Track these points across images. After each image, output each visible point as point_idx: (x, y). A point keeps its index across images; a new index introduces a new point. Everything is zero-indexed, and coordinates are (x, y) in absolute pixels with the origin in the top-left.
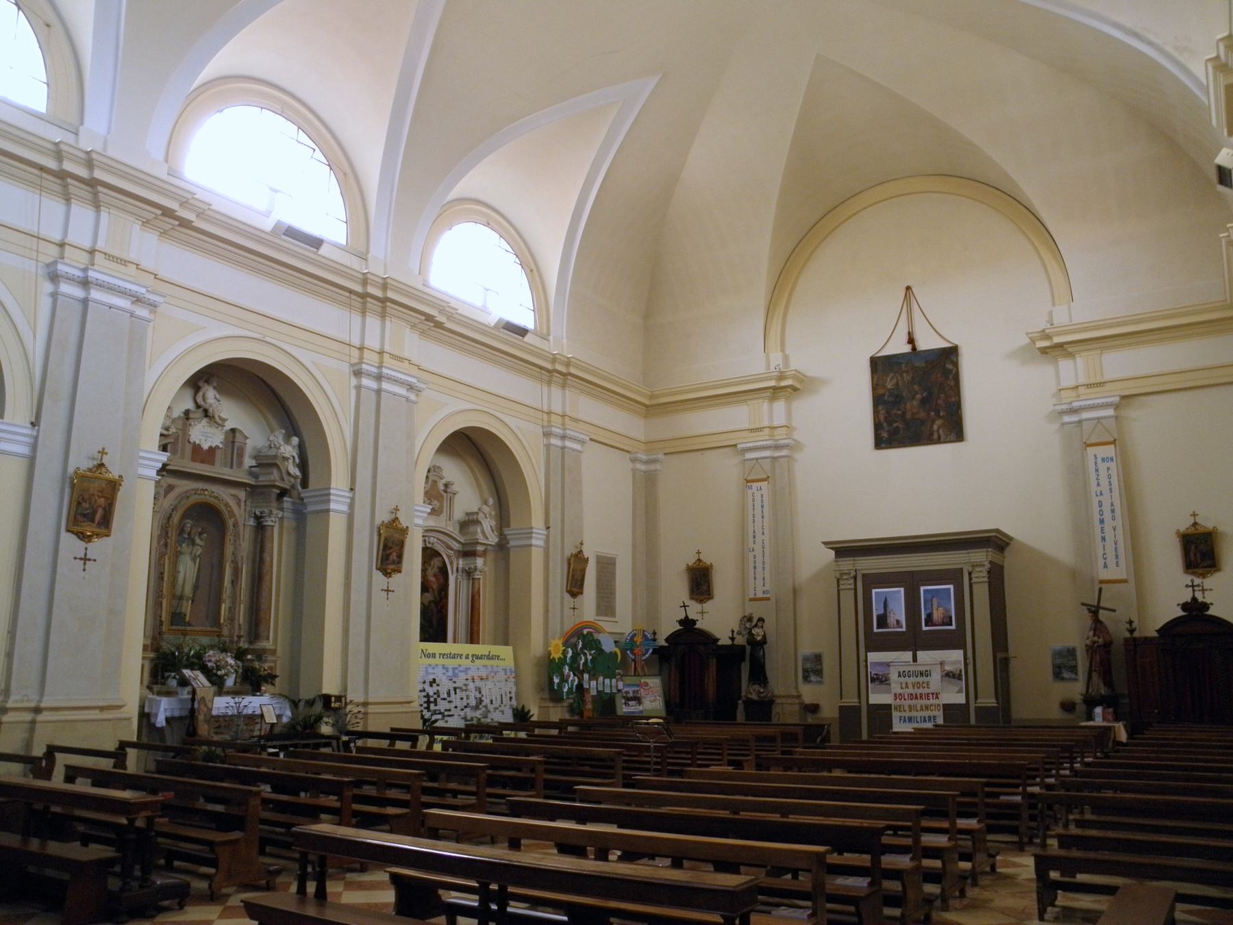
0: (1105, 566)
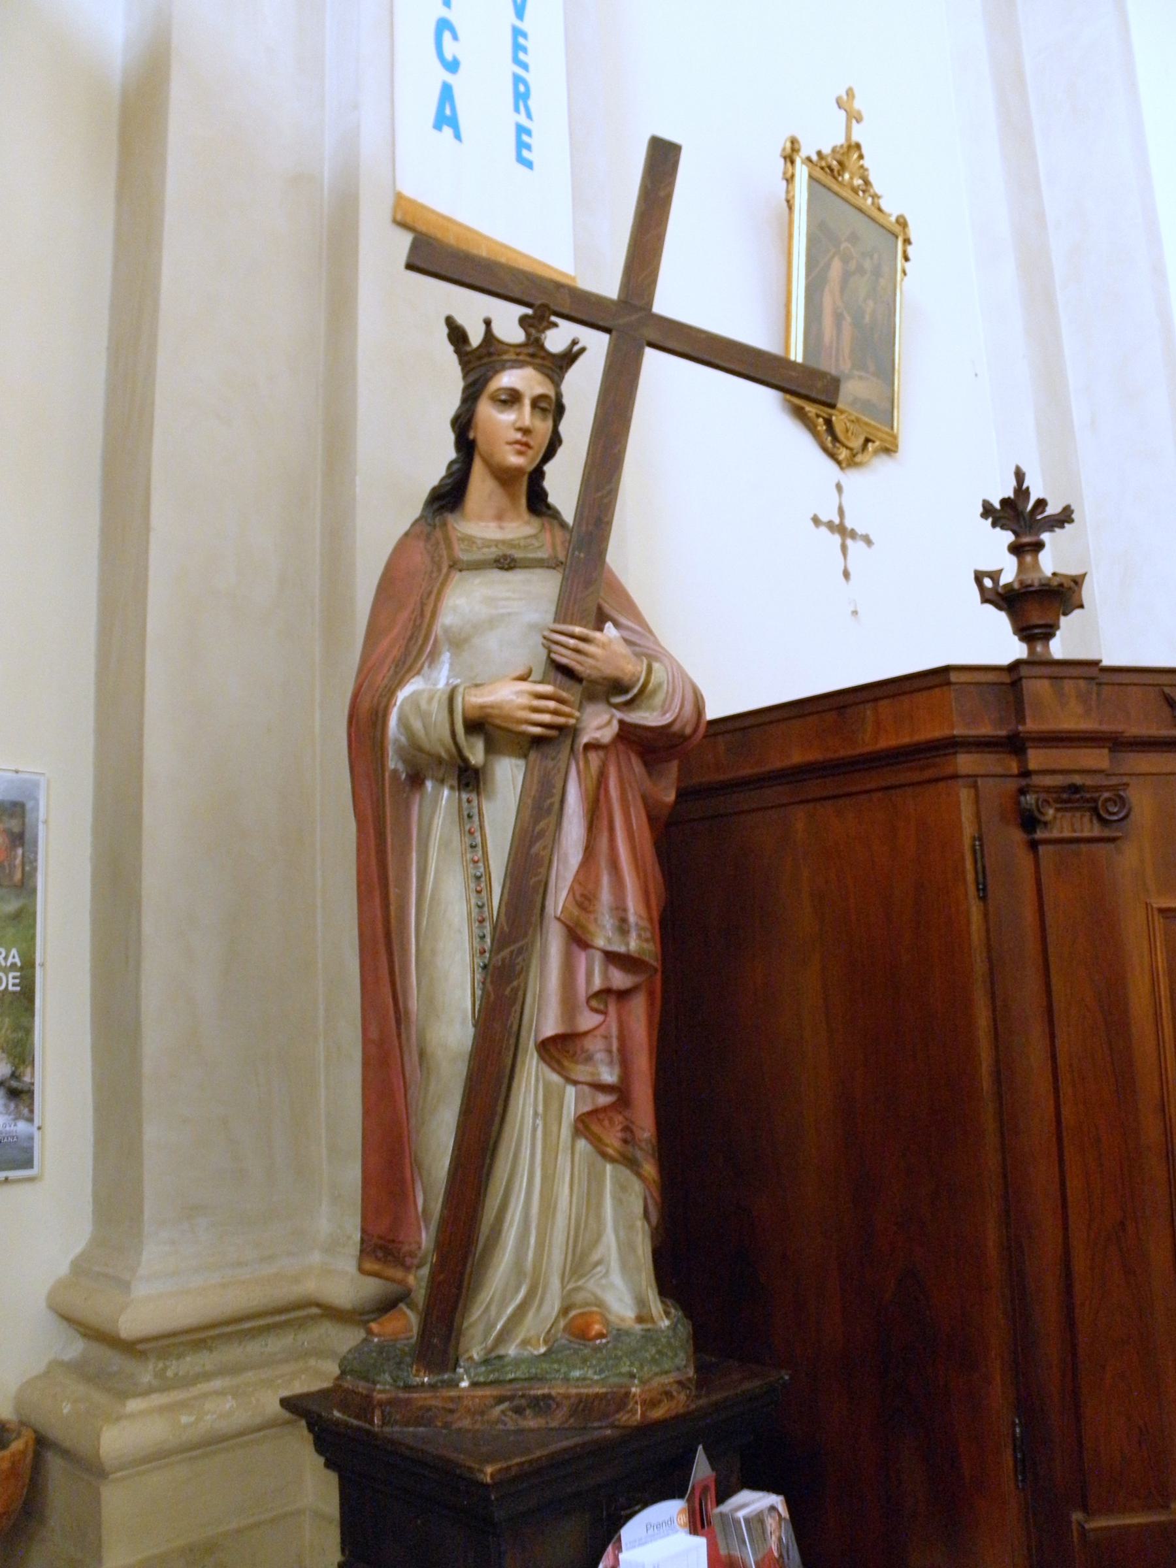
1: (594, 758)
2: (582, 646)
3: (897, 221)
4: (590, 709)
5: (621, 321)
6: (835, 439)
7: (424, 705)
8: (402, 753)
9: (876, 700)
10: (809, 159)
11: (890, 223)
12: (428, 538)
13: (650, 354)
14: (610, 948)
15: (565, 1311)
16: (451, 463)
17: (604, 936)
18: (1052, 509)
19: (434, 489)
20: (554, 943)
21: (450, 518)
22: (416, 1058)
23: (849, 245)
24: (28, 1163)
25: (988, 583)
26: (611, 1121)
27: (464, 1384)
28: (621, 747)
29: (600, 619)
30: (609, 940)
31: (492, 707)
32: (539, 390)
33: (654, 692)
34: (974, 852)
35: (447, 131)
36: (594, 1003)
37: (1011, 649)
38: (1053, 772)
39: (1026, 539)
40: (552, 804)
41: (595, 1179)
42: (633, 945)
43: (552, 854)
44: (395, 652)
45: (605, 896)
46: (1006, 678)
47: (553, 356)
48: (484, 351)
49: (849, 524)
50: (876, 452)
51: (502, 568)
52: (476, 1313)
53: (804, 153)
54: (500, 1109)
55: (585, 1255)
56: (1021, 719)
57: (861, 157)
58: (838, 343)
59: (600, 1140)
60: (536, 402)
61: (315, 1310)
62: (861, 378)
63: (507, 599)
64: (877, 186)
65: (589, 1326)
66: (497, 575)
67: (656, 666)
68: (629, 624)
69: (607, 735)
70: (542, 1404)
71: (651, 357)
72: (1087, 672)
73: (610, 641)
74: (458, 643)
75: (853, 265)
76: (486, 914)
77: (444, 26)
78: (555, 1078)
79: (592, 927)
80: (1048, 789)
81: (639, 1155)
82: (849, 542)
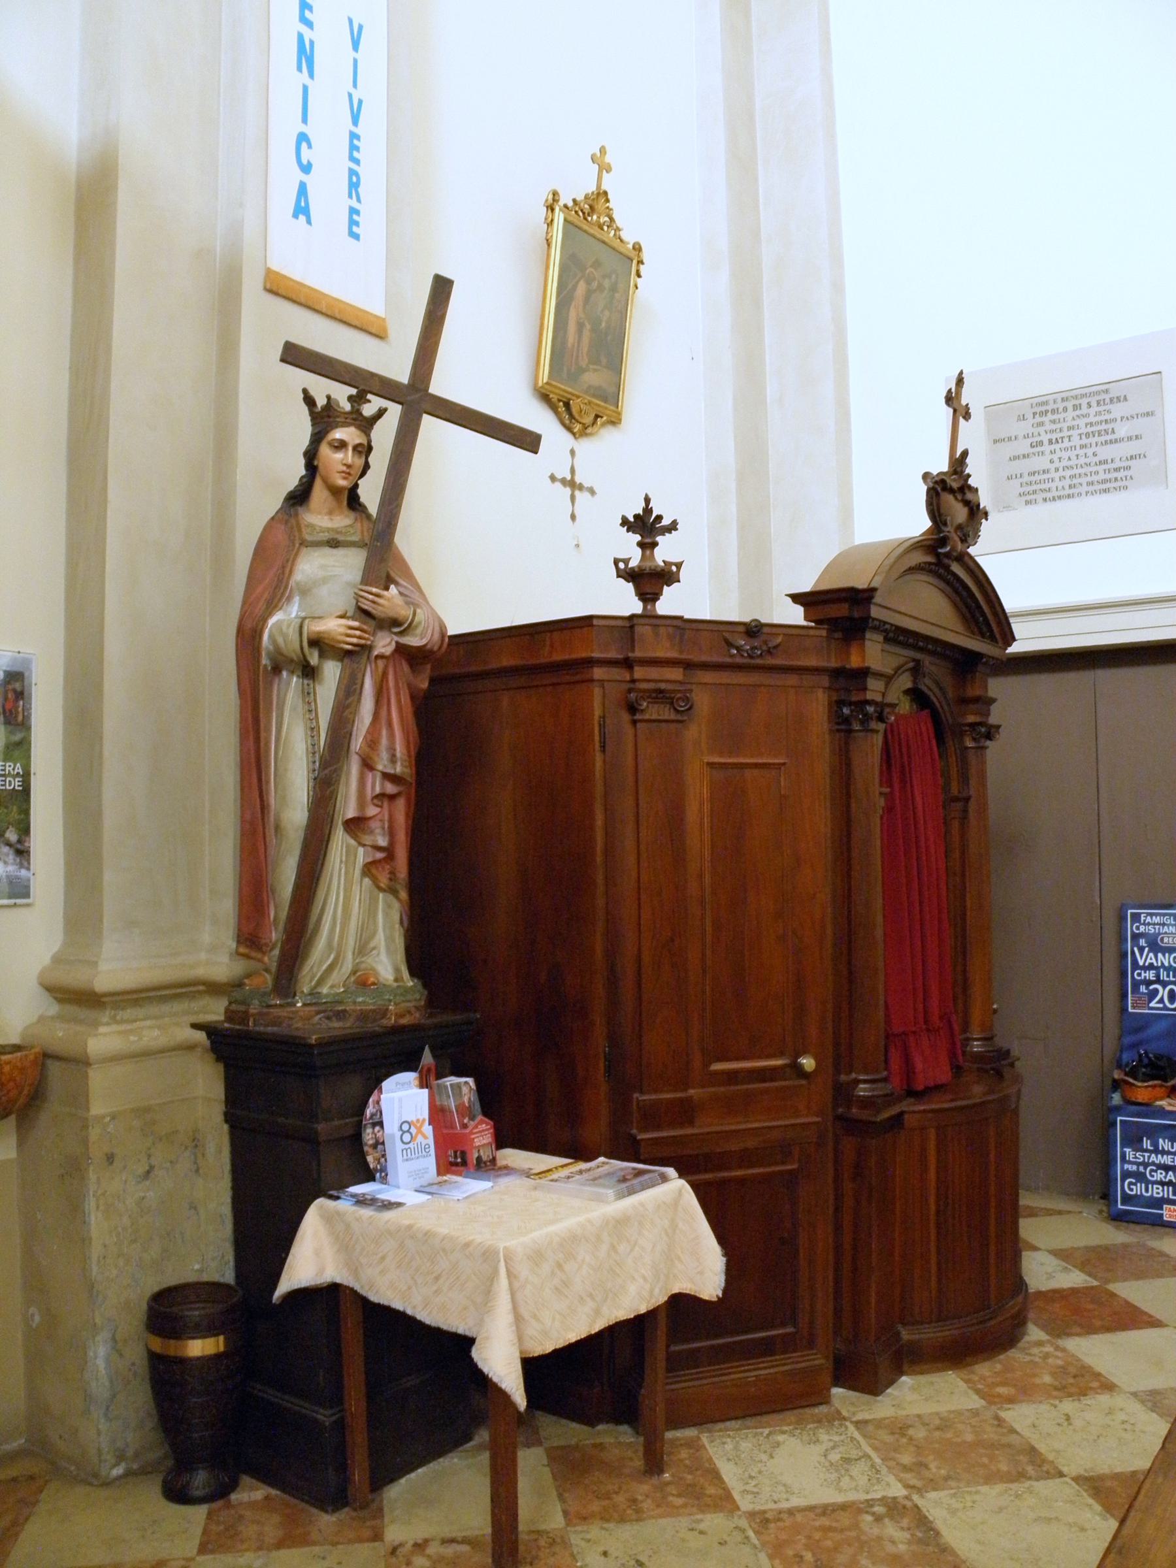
0: (302, 209)
1: (381, 663)
2: (376, 599)
3: (634, 248)
4: (380, 634)
5: (409, 398)
6: (572, 416)
7: (284, 629)
8: (268, 654)
9: (551, 631)
10: (566, 206)
11: (628, 249)
12: (286, 522)
13: (425, 416)
14: (385, 771)
15: (354, 972)
16: (302, 477)
17: (383, 763)
18: (666, 522)
19: (291, 492)
20: (354, 767)
21: (300, 509)
22: (273, 831)
23: (592, 270)
24: (27, 895)
25: (621, 565)
26: (383, 868)
27: (299, 1005)
28: (396, 656)
29: (388, 582)
30: (385, 766)
31: (323, 633)
32: (358, 441)
33: (416, 627)
34: (600, 725)
35: (302, 218)
36: (375, 801)
37: (635, 606)
38: (649, 681)
39: (648, 540)
40: (355, 690)
41: (373, 901)
42: (398, 769)
43: (354, 717)
44: (266, 595)
45: (384, 741)
46: (627, 624)
47: (365, 418)
48: (325, 414)
49: (578, 480)
50: (603, 425)
51: (331, 547)
52: (306, 969)
53: (561, 203)
54: (321, 857)
55: (367, 942)
56: (633, 651)
57: (608, 201)
58: (578, 346)
59: (377, 879)
60: (356, 448)
61: (201, 988)
62: (595, 370)
63: (334, 566)
64: (619, 222)
65: (367, 979)
66: (327, 551)
67: (418, 611)
68: (405, 584)
69: (388, 650)
70: (341, 1015)
71: (426, 419)
72: (675, 623)
73: (393, 597)
74: (305, 592)
75: (595, 285)
76: (316, 749)
77: (303, 138)
78: (352, 842)
79: (376, 759)
80: (644, 691)
81: (398, 887)
82: (577, 493)
